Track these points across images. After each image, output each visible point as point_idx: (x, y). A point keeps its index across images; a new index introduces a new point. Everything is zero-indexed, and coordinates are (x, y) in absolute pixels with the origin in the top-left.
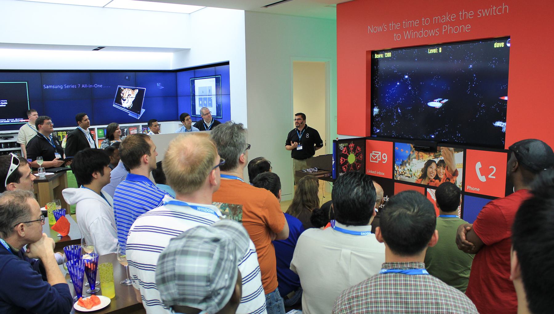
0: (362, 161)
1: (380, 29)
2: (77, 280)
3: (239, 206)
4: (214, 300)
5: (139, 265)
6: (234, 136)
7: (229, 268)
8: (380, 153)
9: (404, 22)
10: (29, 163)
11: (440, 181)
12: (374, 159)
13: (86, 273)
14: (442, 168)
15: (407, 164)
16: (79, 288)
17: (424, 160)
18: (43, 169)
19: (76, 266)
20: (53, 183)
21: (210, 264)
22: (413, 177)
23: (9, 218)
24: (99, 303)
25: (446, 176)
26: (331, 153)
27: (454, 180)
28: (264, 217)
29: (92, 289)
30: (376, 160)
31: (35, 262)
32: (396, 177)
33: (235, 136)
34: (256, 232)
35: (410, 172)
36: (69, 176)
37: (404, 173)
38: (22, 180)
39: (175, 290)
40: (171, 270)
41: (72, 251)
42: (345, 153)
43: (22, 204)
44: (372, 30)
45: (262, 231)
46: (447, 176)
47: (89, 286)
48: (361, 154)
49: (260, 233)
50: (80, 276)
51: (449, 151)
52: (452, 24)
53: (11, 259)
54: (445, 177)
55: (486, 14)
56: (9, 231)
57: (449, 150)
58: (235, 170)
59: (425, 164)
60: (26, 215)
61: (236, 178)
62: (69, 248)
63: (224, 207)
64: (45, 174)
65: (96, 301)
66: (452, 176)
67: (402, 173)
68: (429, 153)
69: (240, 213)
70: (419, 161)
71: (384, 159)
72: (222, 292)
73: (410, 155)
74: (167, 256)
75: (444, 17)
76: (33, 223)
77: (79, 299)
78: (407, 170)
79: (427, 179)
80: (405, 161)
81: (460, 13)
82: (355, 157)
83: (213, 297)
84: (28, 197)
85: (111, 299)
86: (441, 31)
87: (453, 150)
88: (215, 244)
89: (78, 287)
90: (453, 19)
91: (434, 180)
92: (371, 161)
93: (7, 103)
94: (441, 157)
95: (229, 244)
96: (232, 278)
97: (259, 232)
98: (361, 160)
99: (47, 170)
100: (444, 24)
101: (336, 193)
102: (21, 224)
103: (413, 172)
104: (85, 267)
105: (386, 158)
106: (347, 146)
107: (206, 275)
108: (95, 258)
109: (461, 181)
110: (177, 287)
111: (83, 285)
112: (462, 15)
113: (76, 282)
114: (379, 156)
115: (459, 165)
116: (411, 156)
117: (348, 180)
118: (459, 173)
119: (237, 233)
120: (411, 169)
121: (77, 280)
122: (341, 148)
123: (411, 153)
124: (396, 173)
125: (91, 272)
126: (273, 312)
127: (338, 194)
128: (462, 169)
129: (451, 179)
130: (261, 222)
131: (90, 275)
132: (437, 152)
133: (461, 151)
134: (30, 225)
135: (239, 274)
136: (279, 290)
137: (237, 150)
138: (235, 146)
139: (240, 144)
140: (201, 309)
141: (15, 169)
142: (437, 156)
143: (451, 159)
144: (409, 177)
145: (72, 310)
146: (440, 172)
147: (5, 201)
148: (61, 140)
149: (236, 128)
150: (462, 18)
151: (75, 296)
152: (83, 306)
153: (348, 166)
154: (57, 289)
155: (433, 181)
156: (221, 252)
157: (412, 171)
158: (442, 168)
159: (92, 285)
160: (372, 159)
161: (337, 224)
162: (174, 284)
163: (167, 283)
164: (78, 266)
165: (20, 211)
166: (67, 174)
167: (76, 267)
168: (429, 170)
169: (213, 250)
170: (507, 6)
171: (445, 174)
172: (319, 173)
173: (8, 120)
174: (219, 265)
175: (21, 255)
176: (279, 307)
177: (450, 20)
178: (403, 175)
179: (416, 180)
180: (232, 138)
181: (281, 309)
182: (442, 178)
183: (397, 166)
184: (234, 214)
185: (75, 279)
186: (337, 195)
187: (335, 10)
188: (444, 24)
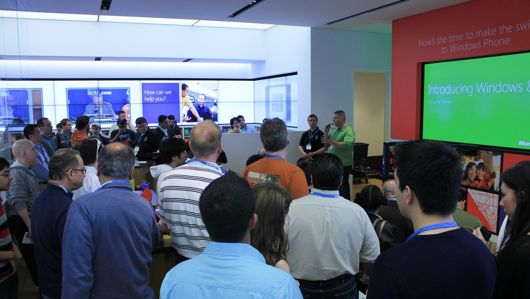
1: (429, 43)
9: (450, 37)
11: (479, 182)
14: (481, 170)
27: (492, 182)
44: (422, 43)
46: (486, 178)
51: (488, 155)
52: (493, 38)
54: (484, 179)
55: (524, 28)
57: (488, 154)
68: (470, 156)
79: (468, 180)
81: (500, 28)
86: (482, 44)
87: (492, 154)
91: (474, 181)
94: (480, 160)
100: (486, 37)
101: (317, 166)
109: (499, 183)
112: (502, 29)
117: (325, 158)
122: (391, 150)
127: (319, 167)
129: (489, 181)
132: (477, 156)
133: (499, 155)
134: (77, 172)
143: (489, 162)
146: (480, 174)
150: (502, 32)
158: (481, 170)
168: (470, 171)
171: (484, 176)
177: (491, 34)
182: (481, 180)
186: (318, 167)
187: (391, 26)
188: (486, 37)
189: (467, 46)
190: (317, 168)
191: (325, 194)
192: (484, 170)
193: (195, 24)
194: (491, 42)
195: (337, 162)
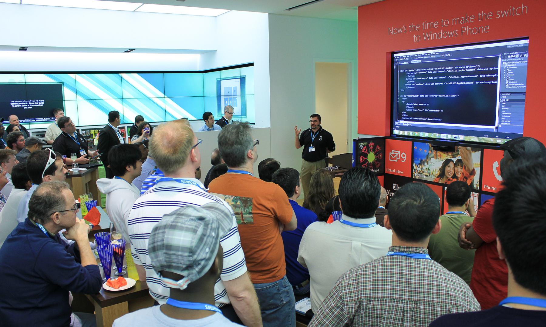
0: (382, 161)
1: (400, 31)
2: (106, 263)
3: (249, 199)
4: (195, 269)
5: (135, 236)
6: (239, 135)
7: (210, 243)
8: (399, 152)
9: (423, 24)
10: (63, 159)
12: (393, 158)
13: (114, 256)
14: (459, 167)
15: (426, 164)
16: (108, 270)
17: (442, 159)
18: (77, 164)
19: (105, 250)
20: (85, 177)
21: (193, 239)
22: (431, 175)
23: (46, 207)
24: (125, 284)
25: (464, 175)
26: (351, 151)
27: (471, 180)
28: (273, 209)
29: (120, 272)
30: (395, 159)
31: (69, 246)
32: (414, 175)
33: (241, 135)
34: (265, 223)
35: (429, 171)
36: (101, 172)
37: (422, 172)
38: (57, 173)
39: (163, 258)
40: (161, 241)
41: (102, 238)
42: (365, 152)
43: (57, 195)
45: (271, 222)
46: (465, 175)
47: (117, 270)
48: (381, 153)
49: (269, 224)
50: (109, 259)
52: (471, 25)
53: (49, 242)
54: (463, 176)
56: (46, 218)
57: (467, 149)
58: (244, 166)
59: (443, 163)
60: (60, 205)
61: (247, 173)
62: (99, 235)
63: (236, 199)
64: (78, 169)
65: (123, 282)
66: (470, 175)
67: (420, 172)
68: (447, 153)
69: (250, 205)
70: (437, 160)
71: (403, 158)
72: (203, 263)
73: (428, 154)
74: (158, 229)
75: (463, 19)
76: (67, 212)
77: (108, 280)
78: (425, 169)
79: (444, 178)
80: (424, 160)
81: (410, 26)
82: (375, 156)
83: (194, 266)
84: (64, 188)
85: (136, 281)
86: (459, 32)
88: (200, 222)
89: (107, 270)
90: (472, 20)
91: (451, 179)
92: (390, 160)
93: (44, 103)
94: (458, 156)
95: (213, 222)
96: (212, 252)
97: (267, 223)
98: (380, 158)
99: (80, 166)
101: (345, 188)
102: (56, 213)
103: (431, 170)
104: (114, 251)
105: (405, 157)
106: (366, 145)
107: (189, 247)
108: (122, 244)
109: (478, 180)
110: (164, 255)
111: (112, 268)
113: (105, 265)
114: (398, 155)
115: (476, 164)
116: (429, 155)
117: (355, 176)
118: (476, 172)
119: (222, 214)
120: (429, 168)
121: (106, 263)
122: (361, 147)
123: (430, 152)
124: (415, 172)
125: (119, 256)
126: (281, 297)
127: (348, 189)
128: (480, 168)
129: (468, 179)
130: (270, 214)
131: (117, 259)
132: (454, 152)
134: (64, 214)
135: (221, 248)
136: (287, 277)
137: (244, 147)
138: (241, 144)
139: (246, 141)
140: (183, 275)
141: (52, 163)
142: (455, 156)
143: (468, 159)
144: (427, 176)
145: (101, 289)
146: (458, 171)
147: (43, 192)
148: (93, 138)
149: (241, 127)
150: (481, 19)
151: (104, 277)
152: (111, 286)
153: (368, 165)
154: (88, 270)
155: (451, 180)
156: (204, 229)
157: (430, 170)
158: (459, 167)
159: (120, 269)
160: (392, 158)
161: (344, 217)
162: (162, 252)
163: (157, 251)
164: (107, 250)
165: (56, 201)
166: (99, 169)
167: (105, 251)
168: (447, 169)
169: (198, 227)
170: (526, 7)
172: (339, 171)
173: (45, 118)
174: (201, 239)
175: (57, 238)
176: (288, 292)
177: (469, 21)
178: (421, 173)
179: (434, 178)
180: (238, 137)
181: (290, 294)
183: (416, 165)
184: (245, 206)
185: (105, 262)
186: (347, 189)
189: (442, 34)
190: (346, 191)
191: (355, 224)
192: (462, 167)
193: (137, 9)
194: (469, 30)
195: (371, 179)
